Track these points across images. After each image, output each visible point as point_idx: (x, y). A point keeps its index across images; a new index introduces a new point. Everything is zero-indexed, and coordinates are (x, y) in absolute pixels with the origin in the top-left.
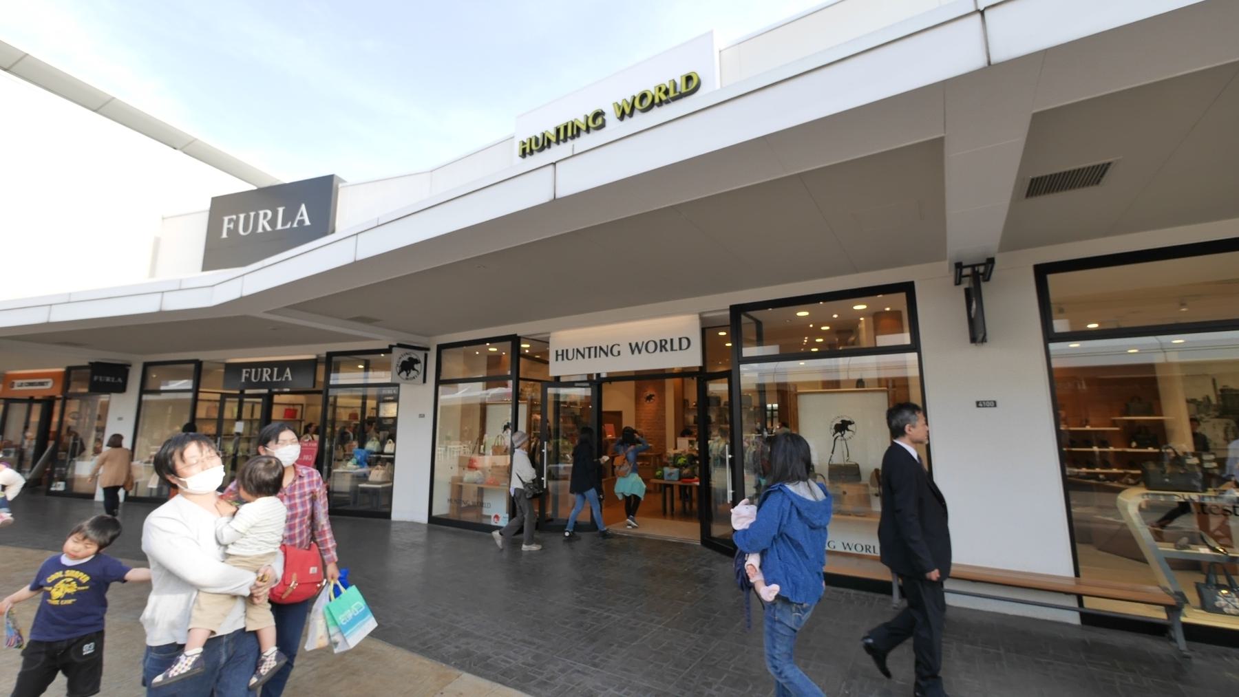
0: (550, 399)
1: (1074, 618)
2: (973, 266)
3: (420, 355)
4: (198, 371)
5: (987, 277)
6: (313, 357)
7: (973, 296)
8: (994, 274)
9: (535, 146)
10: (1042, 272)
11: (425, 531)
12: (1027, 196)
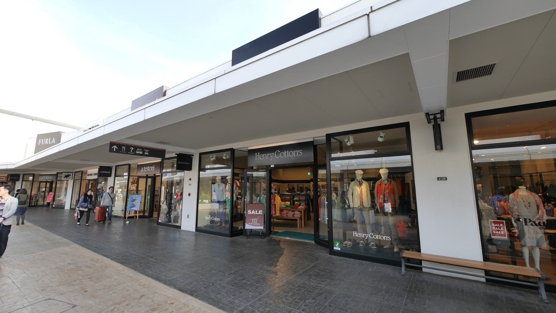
2: (435, 114)
3: (71, 174)
4: (34, 175)
5: (443, 120)
6: (312, 140)
10: (469, 117)
12: (457, 81)
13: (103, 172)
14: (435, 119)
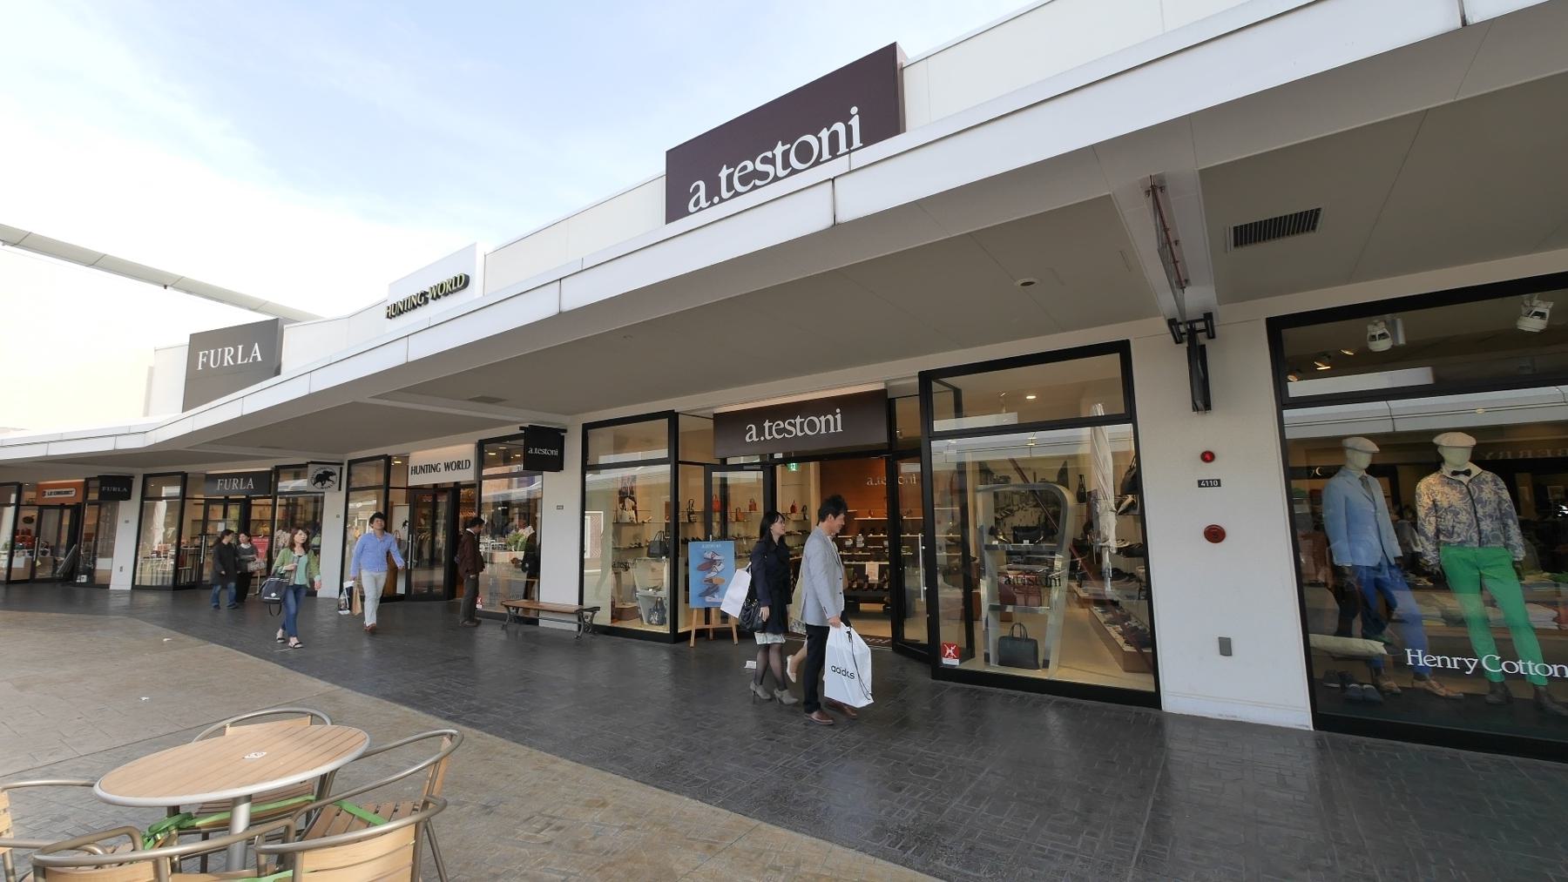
0: (716, 483)
1: (574, 628)
2: (1191, 322)
3: (336, 469)
4: (184, 479)
5: (1212, 336)
6: (881, 386)
7: (1198, 359)
8: (1217, 329)
9: (396, 311)
10: (1276, 326)
11: (1310, 744)
13: (537, 451)
14: (1192, 333)
